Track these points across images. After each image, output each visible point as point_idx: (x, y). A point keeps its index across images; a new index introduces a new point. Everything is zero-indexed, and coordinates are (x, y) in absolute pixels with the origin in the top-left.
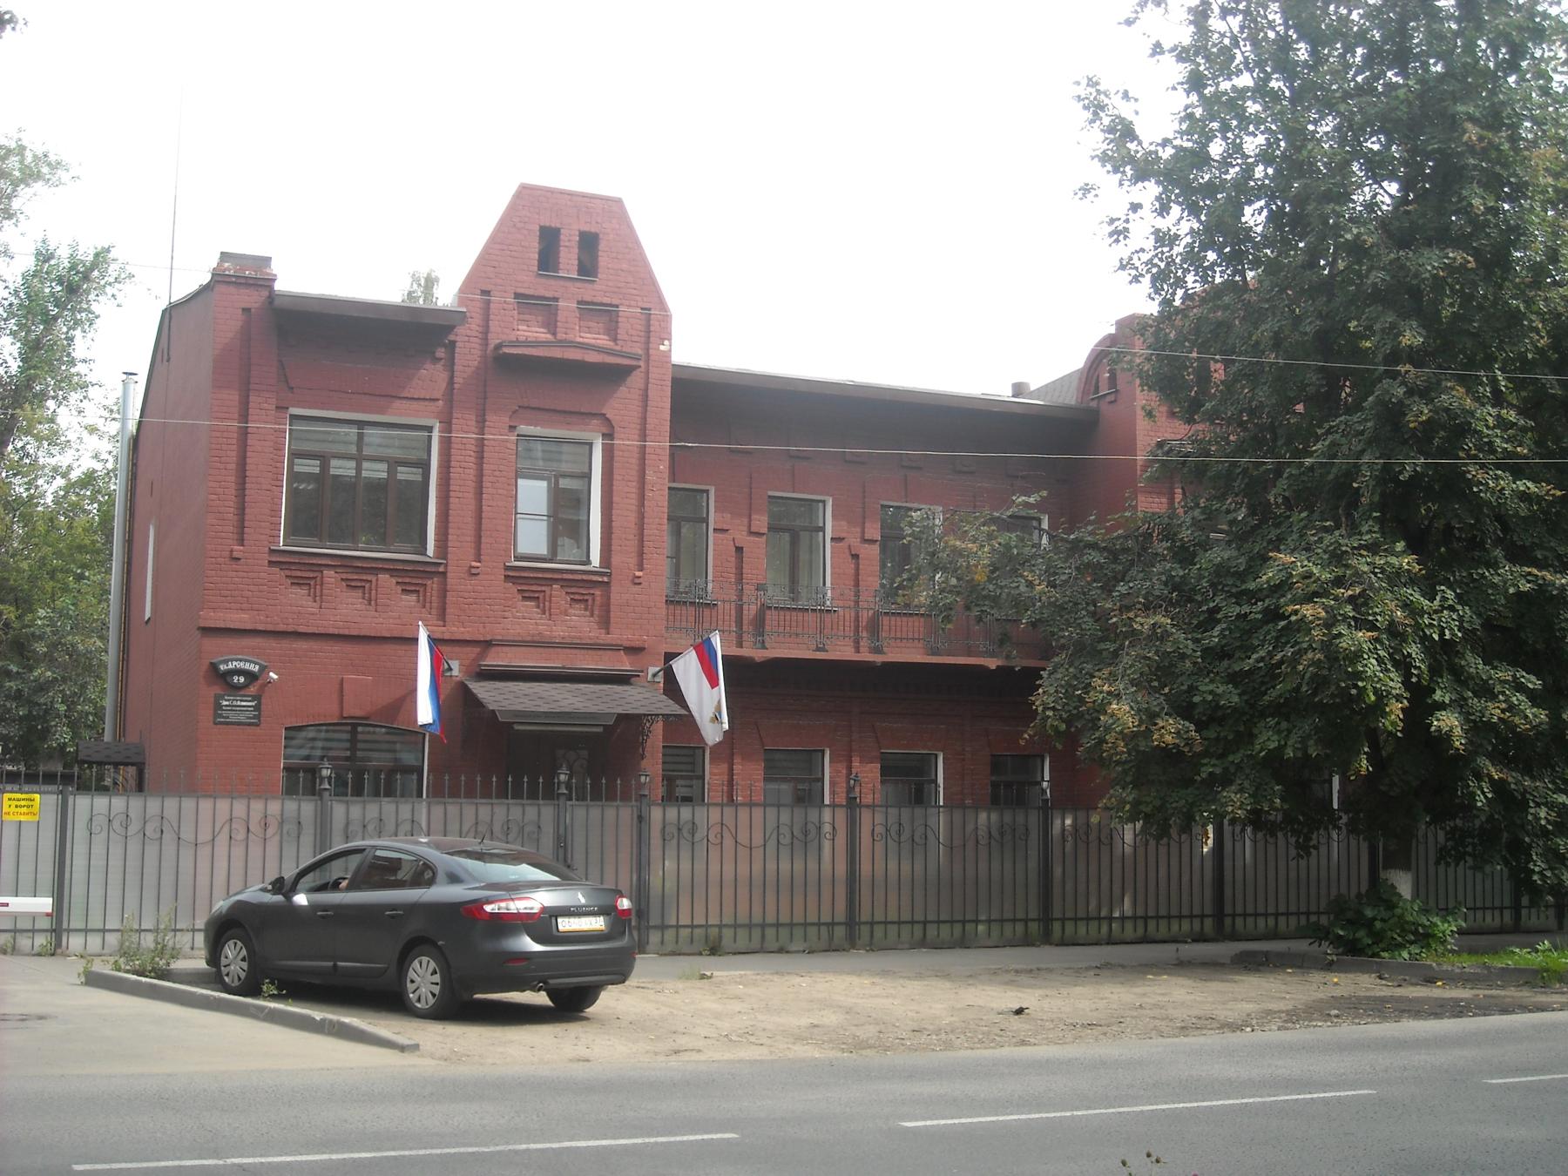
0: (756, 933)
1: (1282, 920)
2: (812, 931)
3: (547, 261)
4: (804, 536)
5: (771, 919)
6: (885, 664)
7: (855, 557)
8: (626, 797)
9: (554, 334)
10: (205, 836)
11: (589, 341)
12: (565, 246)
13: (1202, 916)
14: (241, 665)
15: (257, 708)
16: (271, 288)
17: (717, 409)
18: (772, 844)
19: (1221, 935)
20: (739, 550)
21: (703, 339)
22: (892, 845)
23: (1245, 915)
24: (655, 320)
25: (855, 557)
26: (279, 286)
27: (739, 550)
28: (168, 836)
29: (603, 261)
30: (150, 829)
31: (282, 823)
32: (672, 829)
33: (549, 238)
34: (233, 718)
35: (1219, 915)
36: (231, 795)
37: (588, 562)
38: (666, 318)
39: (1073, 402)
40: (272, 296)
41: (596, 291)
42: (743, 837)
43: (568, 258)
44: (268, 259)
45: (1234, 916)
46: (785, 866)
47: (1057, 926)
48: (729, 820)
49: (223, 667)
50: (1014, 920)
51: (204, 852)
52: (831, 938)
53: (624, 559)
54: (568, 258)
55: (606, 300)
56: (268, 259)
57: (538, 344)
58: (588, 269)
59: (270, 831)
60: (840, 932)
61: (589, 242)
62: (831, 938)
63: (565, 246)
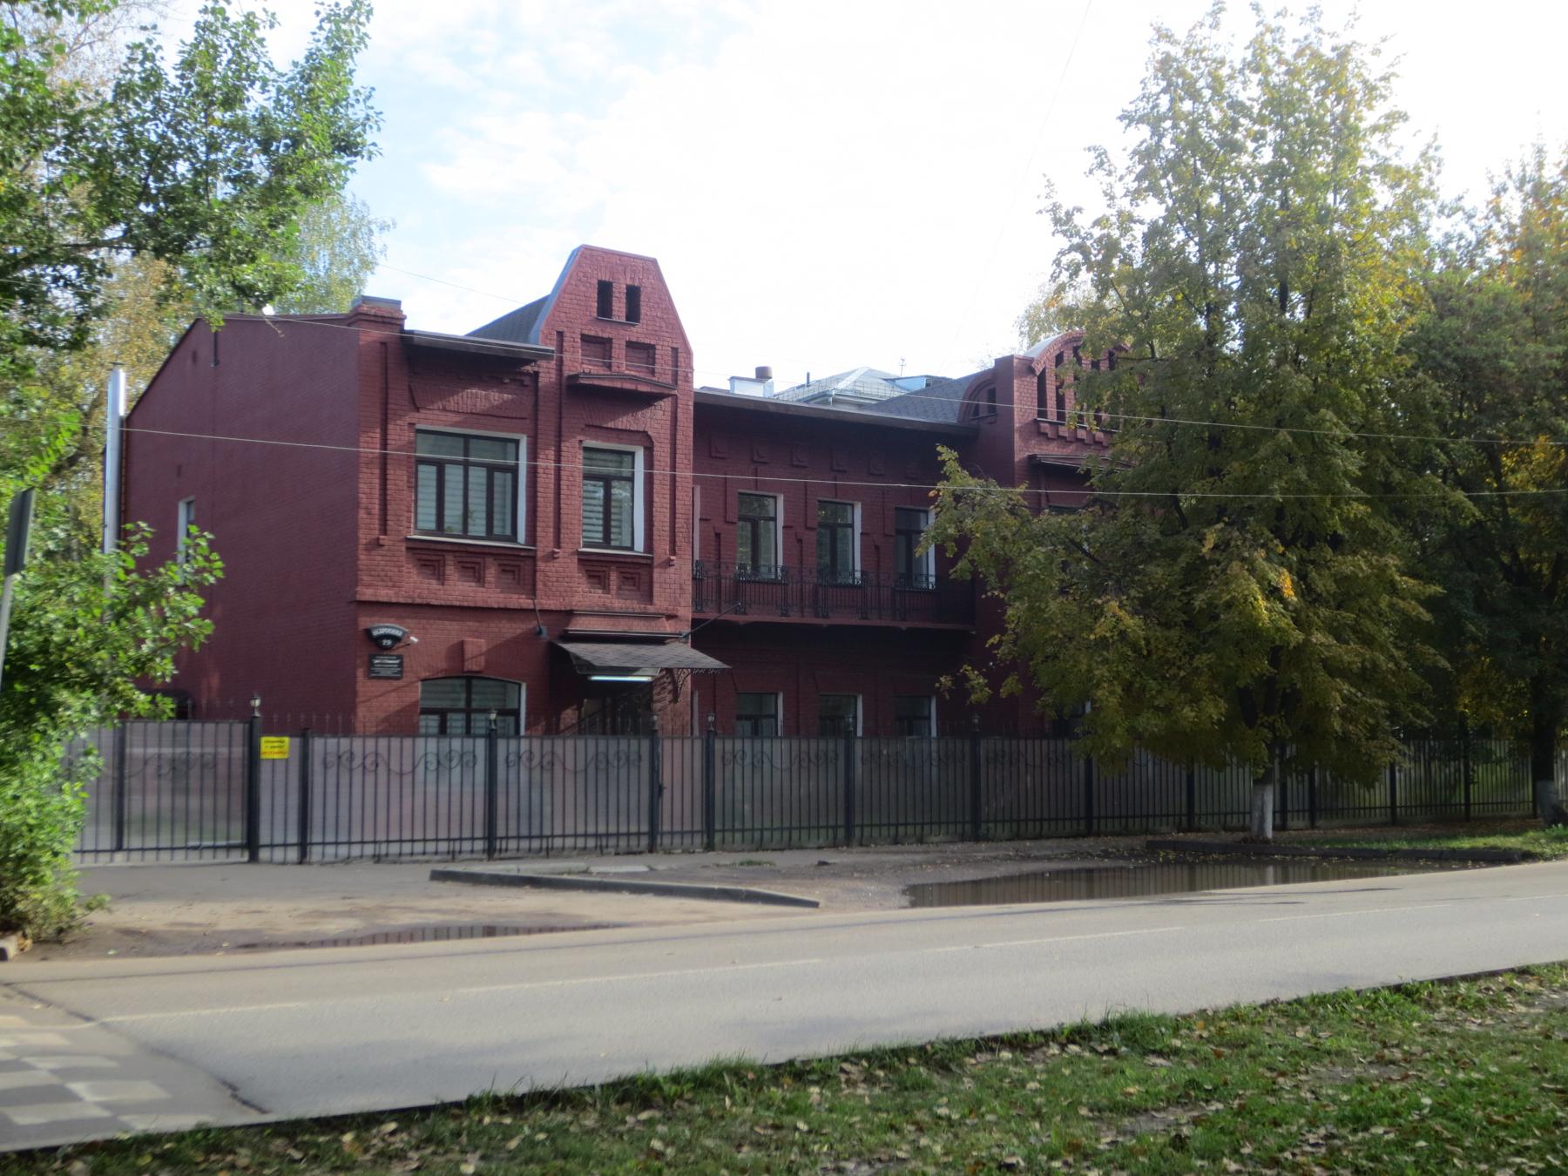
0: (786, 834)
1: (1131, 821)
2: (823, 832)
3: (605, 309)
4: (840, 531)
5: (1068, 815)
6: (831, 627)
7: (800, 541)
8: (636, 732)
9: (609, 366)
10: (407, 768)
11: (624, 370)
12: (617, 295)
13: (692, 833)
14: (389, 631)
15: (401, 665)
16: (402, 326)
17: (743, 432)
18: (795, 767)
19: (1088, 833)
20: (718, 535)
21: (715, 369)
22: (813, 767)
23: (772, 830)
24: (681, 354)
25: (877, 548)
26: (408, 327)
27: (718, 535)
28: (382, 769)
29: (644, 310)
30: (369, 761)
31: (462, 756)
32: (728, 756)
33: (605, 290)
34: (383, 674)
35: (1089, 817)
36: (335, 734)
37: (631, 548)
38: (689, 353)
39: (953, 420)
40: (403, 331)
41: (638, 333)
42: (395, 766)
43: (619, 307)
44: (399, 303)
45: (1099, 818)
46: (166, 801)
47: (857, 831)
48: (1022, 749)
49: (375, 633)
50: (889, 825)
51: (407, 779)
52: (835, 838)
53: (662, 547)
54: (619, 307)
55: (647, 341)
56: (399, 303)
57: (599, 377)
58: (633, 315)
59: (454, 762)
60: (841, 833)
61: (633, 294)
62: (835, 838)
63: (617, 295)
